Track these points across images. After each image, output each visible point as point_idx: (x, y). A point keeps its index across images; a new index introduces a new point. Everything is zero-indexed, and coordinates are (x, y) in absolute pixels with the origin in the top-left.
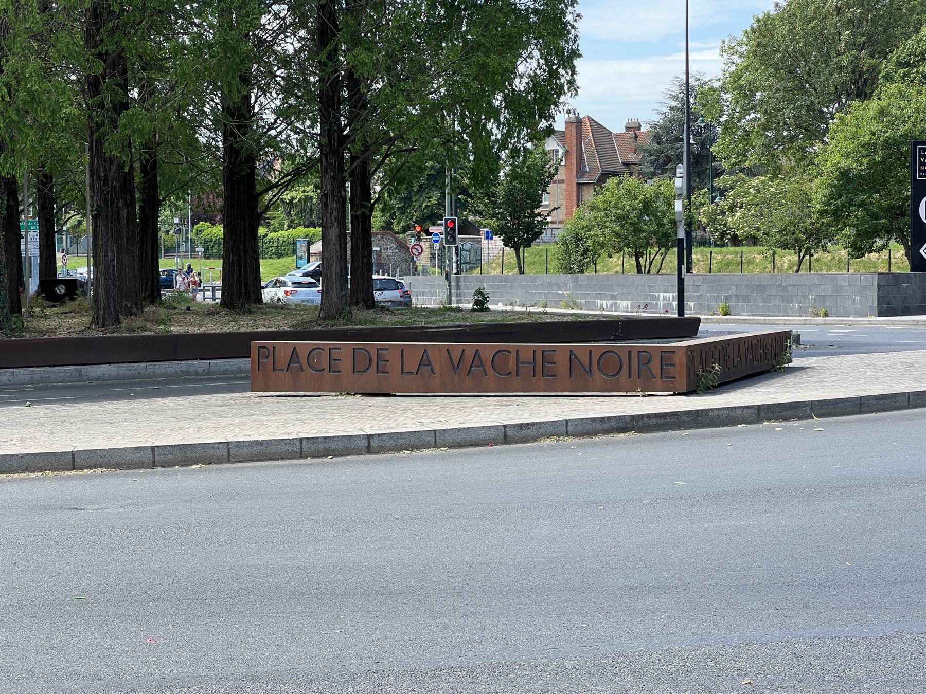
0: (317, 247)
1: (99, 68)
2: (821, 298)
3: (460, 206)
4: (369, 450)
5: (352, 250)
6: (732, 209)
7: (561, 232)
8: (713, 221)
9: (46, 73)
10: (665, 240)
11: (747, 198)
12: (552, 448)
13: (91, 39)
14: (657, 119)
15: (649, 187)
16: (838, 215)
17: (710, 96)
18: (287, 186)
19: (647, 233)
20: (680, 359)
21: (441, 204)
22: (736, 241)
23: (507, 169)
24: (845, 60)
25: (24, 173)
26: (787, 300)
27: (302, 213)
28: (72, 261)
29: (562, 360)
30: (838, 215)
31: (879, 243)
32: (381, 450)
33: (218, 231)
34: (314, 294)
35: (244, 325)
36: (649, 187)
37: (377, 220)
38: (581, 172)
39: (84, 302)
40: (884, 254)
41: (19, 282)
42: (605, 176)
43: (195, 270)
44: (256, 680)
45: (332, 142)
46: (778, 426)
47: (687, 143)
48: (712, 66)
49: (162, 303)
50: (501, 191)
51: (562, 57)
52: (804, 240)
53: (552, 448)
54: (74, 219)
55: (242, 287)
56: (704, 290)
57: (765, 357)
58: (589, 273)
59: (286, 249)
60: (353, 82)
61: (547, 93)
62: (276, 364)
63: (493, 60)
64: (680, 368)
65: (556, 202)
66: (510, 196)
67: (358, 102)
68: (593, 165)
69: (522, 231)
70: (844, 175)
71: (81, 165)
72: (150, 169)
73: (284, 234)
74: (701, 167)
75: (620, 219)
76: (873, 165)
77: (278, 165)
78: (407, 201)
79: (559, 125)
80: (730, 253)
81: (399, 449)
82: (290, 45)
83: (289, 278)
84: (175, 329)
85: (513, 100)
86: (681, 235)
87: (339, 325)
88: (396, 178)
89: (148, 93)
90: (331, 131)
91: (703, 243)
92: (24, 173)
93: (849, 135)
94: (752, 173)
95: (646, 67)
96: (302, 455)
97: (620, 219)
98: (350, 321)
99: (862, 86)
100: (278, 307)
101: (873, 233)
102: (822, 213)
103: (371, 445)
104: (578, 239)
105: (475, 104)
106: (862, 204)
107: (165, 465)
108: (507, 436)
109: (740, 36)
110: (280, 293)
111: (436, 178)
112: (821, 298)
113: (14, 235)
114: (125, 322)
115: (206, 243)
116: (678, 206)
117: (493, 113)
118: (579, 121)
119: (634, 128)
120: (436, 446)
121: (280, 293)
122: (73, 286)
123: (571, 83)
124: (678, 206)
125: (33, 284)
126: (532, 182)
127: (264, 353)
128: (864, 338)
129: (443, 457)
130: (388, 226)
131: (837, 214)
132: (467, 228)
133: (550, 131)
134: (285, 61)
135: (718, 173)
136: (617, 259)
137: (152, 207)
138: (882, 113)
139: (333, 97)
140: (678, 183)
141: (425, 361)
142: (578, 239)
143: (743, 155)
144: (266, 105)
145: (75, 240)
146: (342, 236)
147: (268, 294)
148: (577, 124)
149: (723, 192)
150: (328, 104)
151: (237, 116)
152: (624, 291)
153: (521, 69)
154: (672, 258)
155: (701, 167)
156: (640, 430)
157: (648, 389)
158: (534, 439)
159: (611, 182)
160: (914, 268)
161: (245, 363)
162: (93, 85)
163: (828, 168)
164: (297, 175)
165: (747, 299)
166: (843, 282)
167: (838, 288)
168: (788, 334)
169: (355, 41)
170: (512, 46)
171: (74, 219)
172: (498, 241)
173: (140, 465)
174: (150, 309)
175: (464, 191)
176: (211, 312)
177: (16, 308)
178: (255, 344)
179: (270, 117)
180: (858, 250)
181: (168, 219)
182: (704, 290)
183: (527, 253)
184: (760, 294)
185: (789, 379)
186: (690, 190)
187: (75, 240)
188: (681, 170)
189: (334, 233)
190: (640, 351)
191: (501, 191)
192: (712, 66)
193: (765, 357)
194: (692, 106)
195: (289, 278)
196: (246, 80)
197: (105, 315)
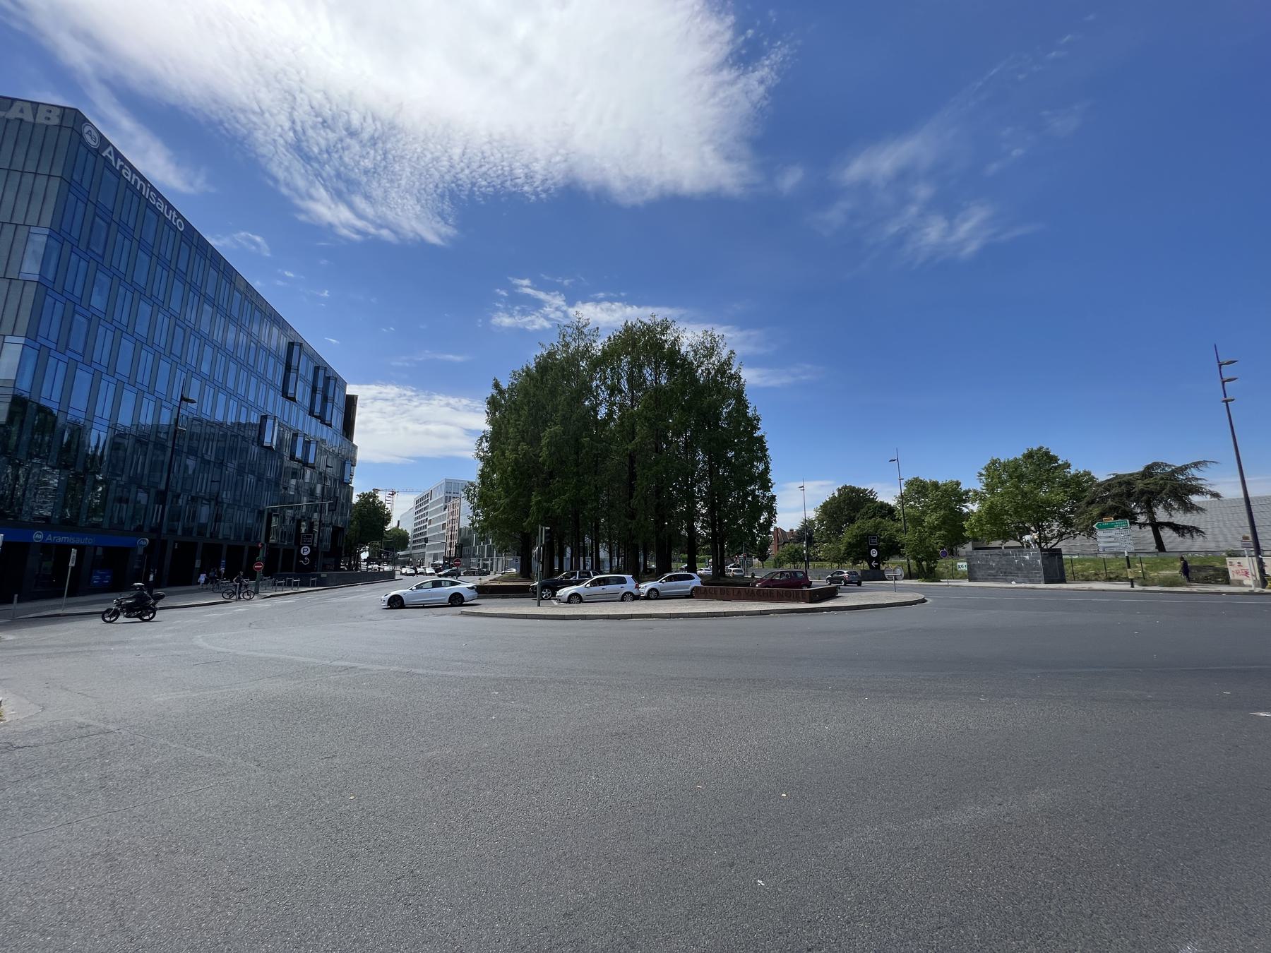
5: (1091, 590)
10: (802, 560)
11: (821, 550)
14: (796, 528)
17: (812, 522)
19: (795, 557)
23: (557, 428)
45: (714, 534)
47: (806, 534)
48: (812, 515)
59: (703, 561)
61: (769, 522)
62: (1239, 479)
65: (772, 550)
80: (819, 564)
85: (760, 525)
88: (731, 543)
93: (849, 534)
105: (751, 527)
108: (761, 613)
122: (652, 570)
126: (765, 544)
131: (848, 554)
144: (698, 526)
148: (776, 529)
151: (691, 529)
155: (810, 541)
157: (798, 600)
162: (656, 522)
164: (705, 543)
181: (674, 554)
192: (812, 515)
194: (807, 525)
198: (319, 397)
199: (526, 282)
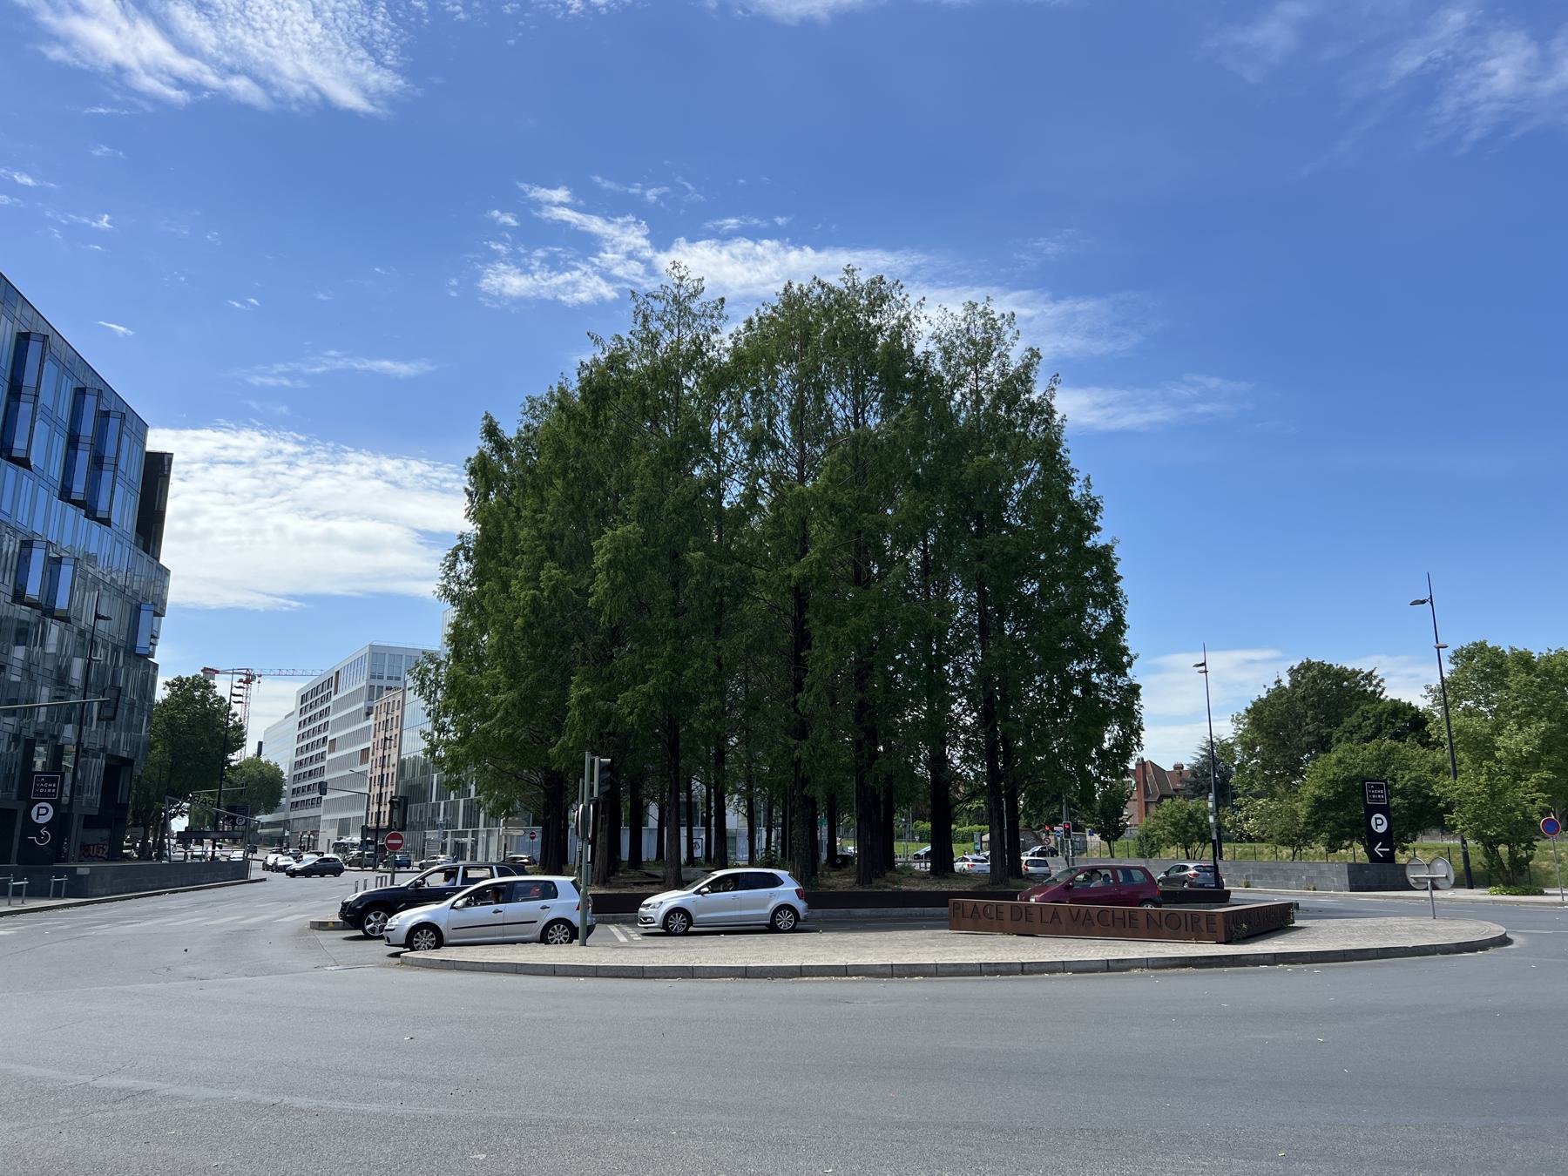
0: (986, 837)
1: (862, 735)
2: (1311, 878)
3: (1072, 815)
4: (1023, 972)
6: (1247, 819)
7: (1137, 833)
8: (1234, 826)
9: (833, 738)
10: (1204, 838)
11: (1253, 813)
12: (1138, 976)
13: (858, 720)
15: (1191, 805)
16: (1317, 824)
17: (1226, 748)
18: (969, 801)
19: (1189, 832)
20: (1219, 920)
21: (1061, 812)
22: (1250, 839)
24: (1311, 728)
25: (819, 794)
26: (1288, 879)
27: (977, 817)
28: (845, 842)
29: (1142, 919)
30: (1317, 824)
31: (1346, 843)
32: (1031, 973)
33: (928, 826)
34: (986, 867)
35: (944, 887)
36: (1191, 805)
37: (1022, 823)
38: (1147, 794)
39: (852, 869)
40: (1350, 851)
41: (817, 856)
42: (1162, 797)
43: (912, 851)
44: (957, 1127)
45: (994, 774)
46: (1289, 968)
47: (1213, 776)
48: (1226, 731)
49: (896, 871)
50: (1097, 806)
51: (1132, 728)
52: (1296, 839)
53: (1138, 976)
54: (847, 819)
55: (942, 860)
56: (1231, 871)
57: (1277, 920)
58: (1156, 858)
60: (1006, 742)
61: (1125, 747)
63: (1091, 730)
64: (1220, 926)
65: (1132, 814)
66: (1103, 813)
67: (1009, 754)
68: (1155, 789)
69: (1112, 832)
70: (1318, 799)
71: (851, 786)
72: (889, 791)
73: (966, 829)
74: (1224, 793)
75: (1173, 824)
76: (1337, 793)
77: (961, 789)
78: (1040, 811)
79: (1132, 766)
80: (1247, 847)
81: (1041, 972)
82: (969, 721)
83: (970, 859)
84: (904, 888)
86: (1215, 837)
87: (1002, 889)
88: (1033, 798)
89: (888, 749)
90: (992, 767)
91: (1229, 840)
92: (819, 794)
94: (1257, 796)
95: (1182, 730)
96: (981, 974)
97: (1173, 824)
98: (1008, 886)
99: (1324, 745)
100: (964, 875)
101: (1342, 837)
102: (1306, 824)
103: (1024, 969)
104: (1147, 837)
106: (1332, 818)
107: (899, 976)
108: (1109, 966)
109: (1243, 713)
110: (965, 865)
111: (1057, 798)
112: (1311, 878)
113: (814, 829)
114: (876, 882)
115: (921, 833)
116: (1211, 819)
117: (1092, 761)
118: (1144, 764)
119: (1179, 767)
120: (1064, 971)
121: (965, 865)
122: (847, 859)
123: (1138, 744)
124: (1211, 819)
125: (824, 856)
126: (1115, 803)
127: (956, 906)
128: (1341, 906)
129: (1069, 979)
130: (1028, 825)
132: (1077, 828)
133: (1126, 772)
134: (965, 729)
135: (1235, 796)
136: (1173, 850)
137: (890, 813)
138: (1340, 761)
139: (991, 749)
140: (1210, 805)
141: (1055, 915)
142: (1147, 837)
143: (1251, 784)
144: (955, 755)
145: (847, 831)
146: (1002, 834)
147: (958, 866)
148: (1142, 764)
149: (1239, 808)
150: (990, 755)
151: (939, 762)
152: (1168, 862)
153: (1107, 736)
154: (1209, 850)
155: (1224, 793)
156: (1196, 966)
157: (1199, 937)
158: (1127, 969)
159: (1167, 801)
160: (1372, 860)
161: (945, 910)
162: (858, 745)
163: (1307, 795)
164: (972, 796)
165: (1260, 877)
166: (1324, 867)
167: (1321, 872)
168: (1289, 906)
169: (1006, 719)
170: (1102, 721)
171: (847, 819)
172: (1097, 837)
173: (884, 975)
174: (889, 874)
175: (1075, 806)
176: (923, 877)
177: (814, 873)
178: (952, 900)
179: (957, 762)
180: (1333, 847)
181: (899, 821)
182: (1231, 871)
183: (1115, 845)
184: (1269, 874)
185: (1293, 935)
186: (1217, 806)
187: (847, 831)
188: (1211, 797)
189: (996, 832)
190: (1192, 914)
191: (1097, 806)
192: (1226, 731)
193: (1277, 920)
194: (1216, 754)
195: (970, 859)
196: (943, 742)
197: (865, 877)
198: (83, 457)
199: (560, 195)
